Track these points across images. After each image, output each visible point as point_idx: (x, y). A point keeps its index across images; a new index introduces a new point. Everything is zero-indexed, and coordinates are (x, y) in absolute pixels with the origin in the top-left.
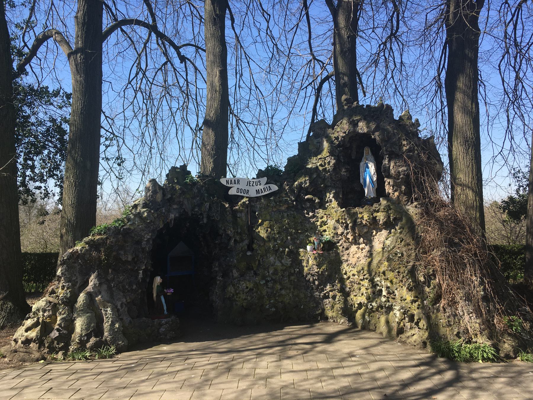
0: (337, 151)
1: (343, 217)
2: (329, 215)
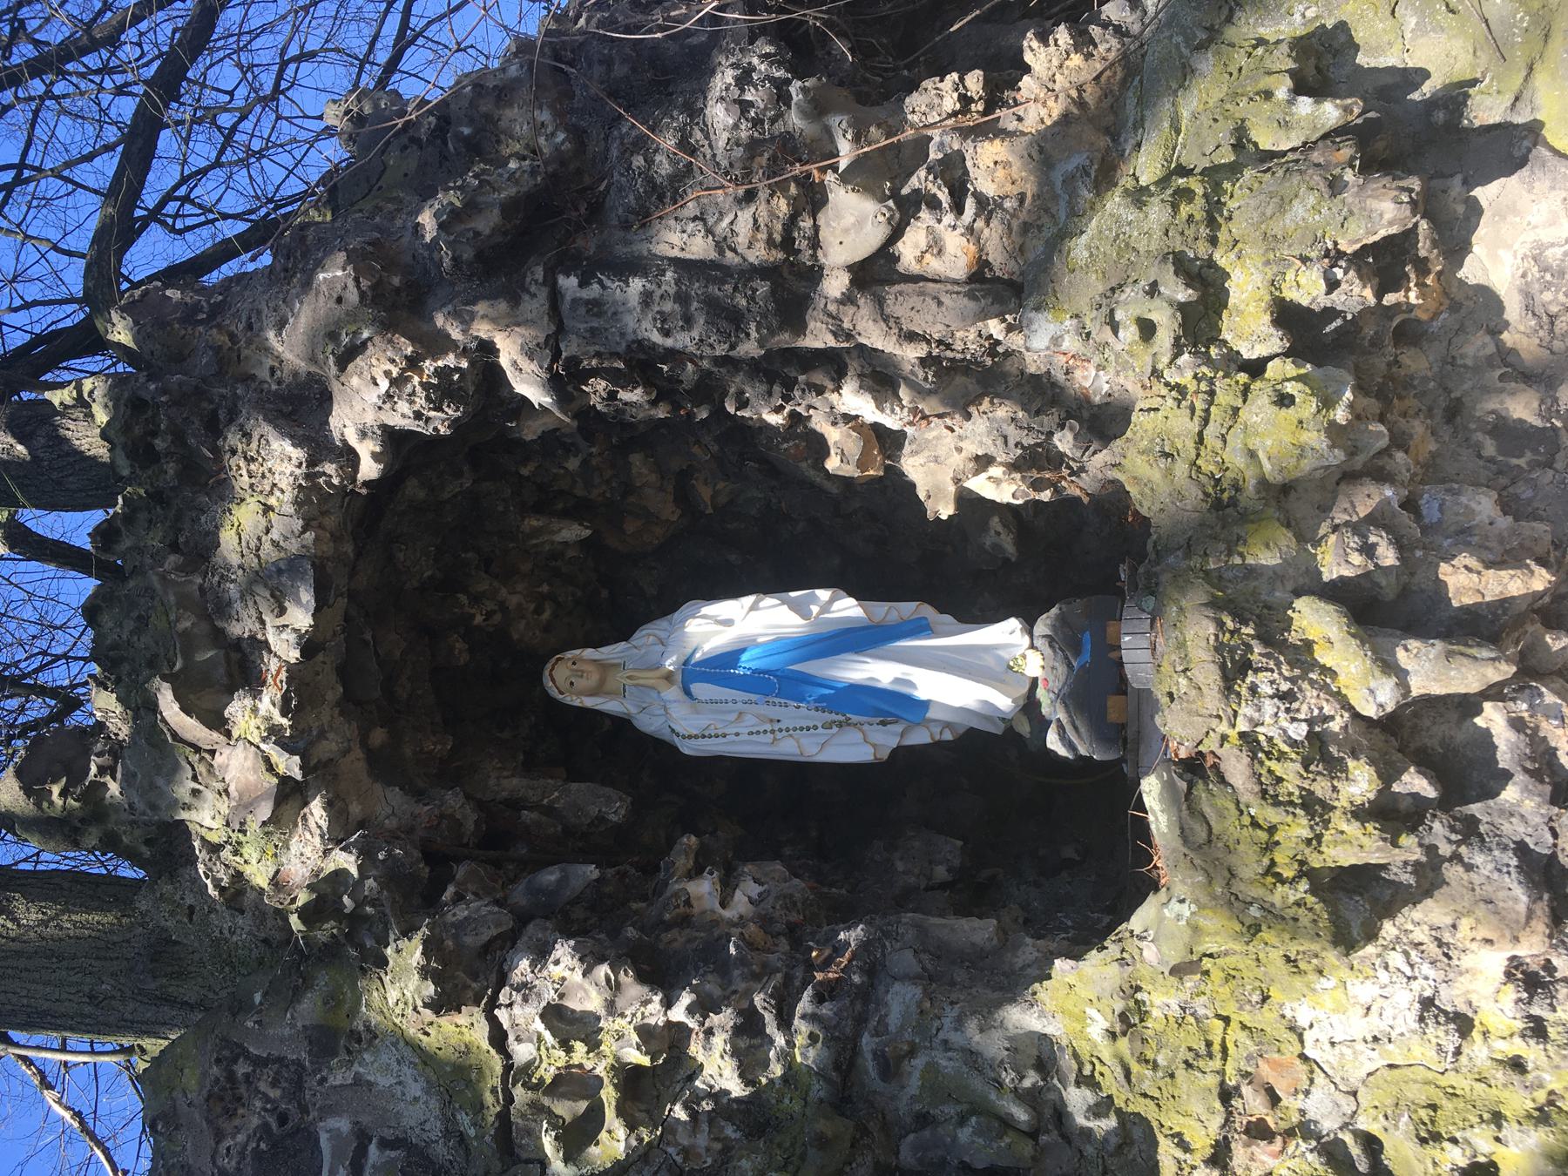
0: (461, 912)
1: (1290, 773)
2: (1227, 1095)
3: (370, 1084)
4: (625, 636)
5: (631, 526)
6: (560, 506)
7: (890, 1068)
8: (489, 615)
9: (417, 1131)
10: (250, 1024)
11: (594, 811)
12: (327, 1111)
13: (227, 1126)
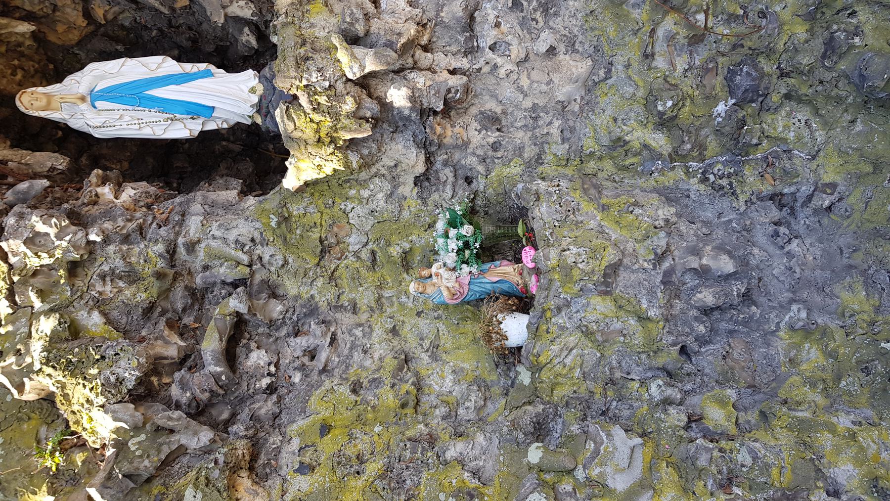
4: (60, 80)
5: (60, 28)
7: (191, 247)
11: (49, 164)
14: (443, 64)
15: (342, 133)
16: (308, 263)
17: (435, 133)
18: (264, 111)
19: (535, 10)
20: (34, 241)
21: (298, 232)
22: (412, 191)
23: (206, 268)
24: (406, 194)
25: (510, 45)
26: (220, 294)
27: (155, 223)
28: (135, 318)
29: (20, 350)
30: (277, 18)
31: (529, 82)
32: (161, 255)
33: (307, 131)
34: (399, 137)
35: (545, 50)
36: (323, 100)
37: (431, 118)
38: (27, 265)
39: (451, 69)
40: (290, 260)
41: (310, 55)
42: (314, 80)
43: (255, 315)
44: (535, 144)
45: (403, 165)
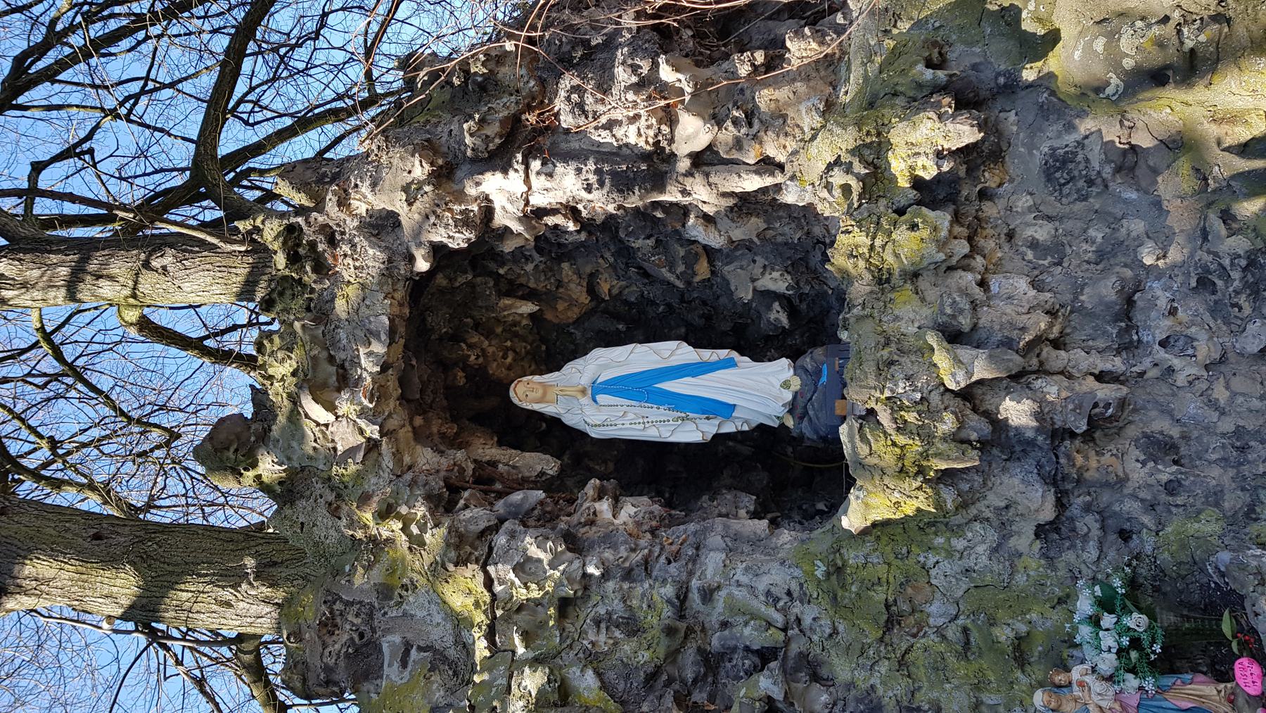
3: (412, 616)
5: (561, 306)
6: (520, 293)
7: (708, 595)
8: (478, 357)
9: (439, 641)
10: (343, 582)
11: (539, 468)
12: (387, 631)
13: (329, 640)
14: (1084, 366)
15: (935, 461)
16: (867, 636)
17: (1074, 465)
18: (799, 411)
19: (1237, 293)
20: (525, 568)
21: (854, 589)
22: (1031, 545)
23: (725, 625)
24: (1021, 549)
25: (1193, 340)
26: (743, 664)
27: (663, 557)
28: (635, 684)
29: (496, 707)
30: (850, 310)
31: (1228, 393)
32: (669, 601)
33: (887, 457)
34: (1015, 468)
35: (1256, 350)
36: (911, 417)
37: (1067, 443)
38: (513, 596)
39: (1097, 372)
40: (841, 628)
41: (896, 358)
42: (901, 391)
43: (792, 704)
44: (1243, 489)
45: (1019, 507)
